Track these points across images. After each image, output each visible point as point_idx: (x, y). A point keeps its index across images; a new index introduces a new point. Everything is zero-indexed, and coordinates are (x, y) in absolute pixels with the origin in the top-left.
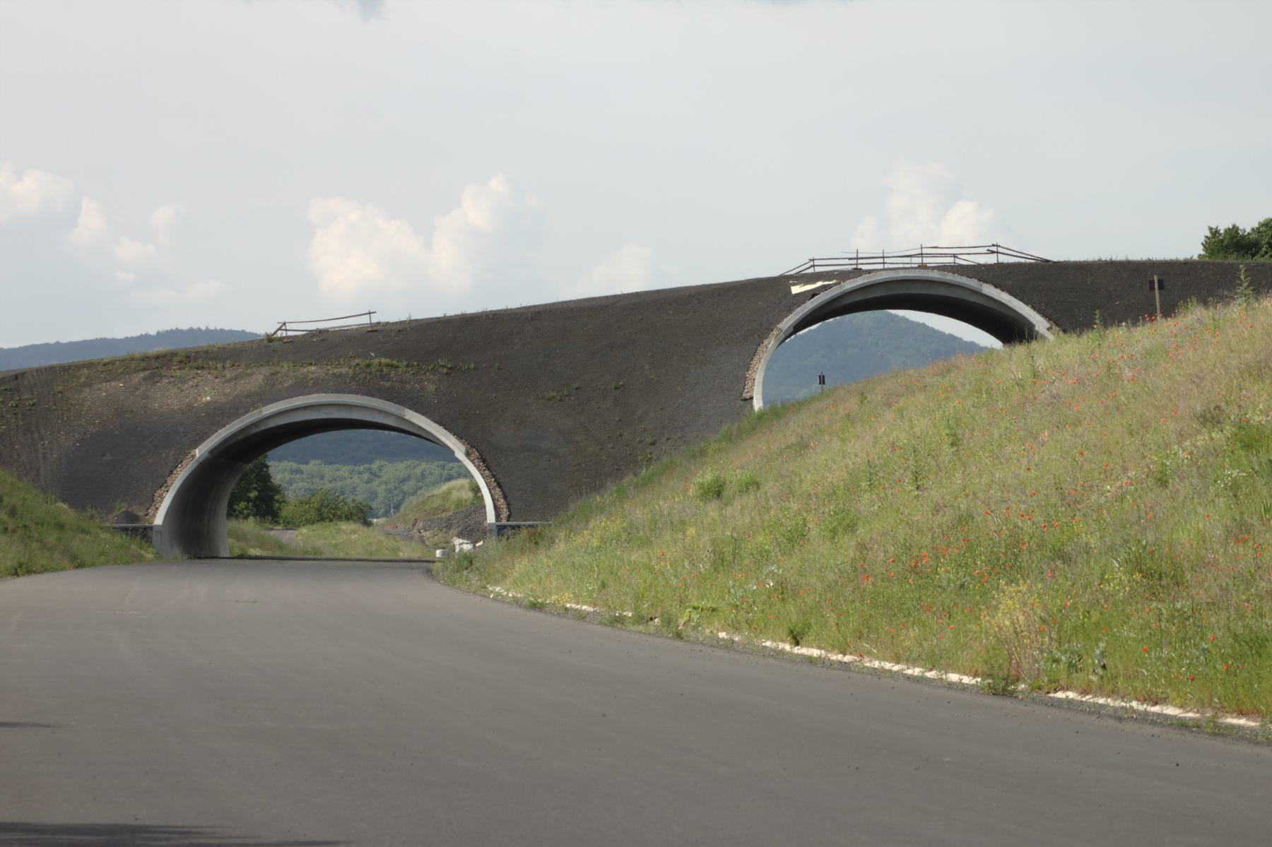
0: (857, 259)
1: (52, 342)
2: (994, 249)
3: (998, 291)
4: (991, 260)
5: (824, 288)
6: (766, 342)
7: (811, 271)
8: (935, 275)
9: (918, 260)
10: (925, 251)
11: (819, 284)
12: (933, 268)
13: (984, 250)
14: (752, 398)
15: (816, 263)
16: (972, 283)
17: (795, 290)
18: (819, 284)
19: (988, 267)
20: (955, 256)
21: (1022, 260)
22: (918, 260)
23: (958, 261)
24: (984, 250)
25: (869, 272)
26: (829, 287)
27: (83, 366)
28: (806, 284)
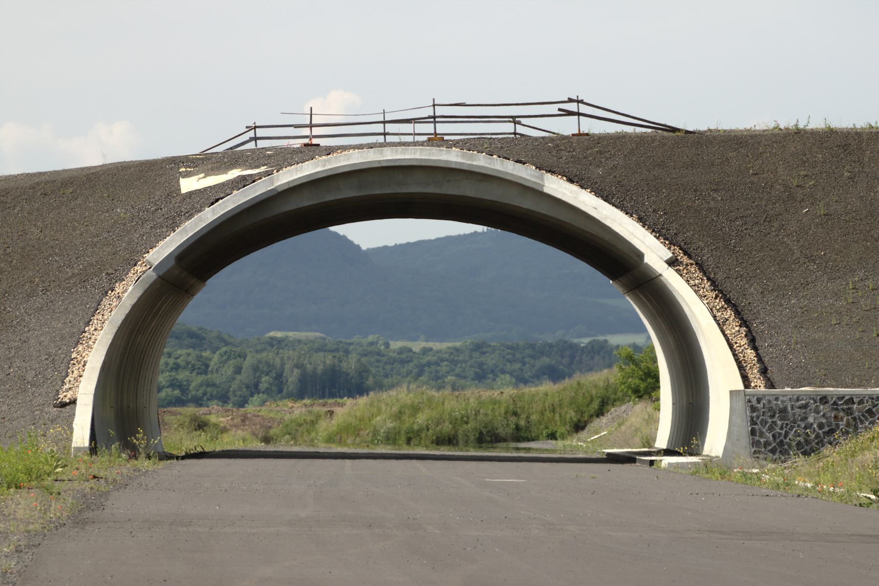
0: (311, 126)
1: (356, 242)
2: (572, 107)
3: (574, 188)
4: (567, 127)
5: (242, 182)
6: (119, 288)
7: (251, 145)
8: (453, 157)
9: (429, 128)
10: (440, 111)
11: (234, 174)
12: (456, 144)
13: (553, 109)
14: (73, 402)
15: (260, 133)
16: (526, 173)
17: (188, 185)
18: (234, 174)
19: (558, 142)
20: (514, 120)
21: (629, 129)
22: (429, 128)
23: (520, 129)
24: (553, 109)
25: (329, 151)
26: (253, 179)
27: (714, 317)
28: (208, 173)
